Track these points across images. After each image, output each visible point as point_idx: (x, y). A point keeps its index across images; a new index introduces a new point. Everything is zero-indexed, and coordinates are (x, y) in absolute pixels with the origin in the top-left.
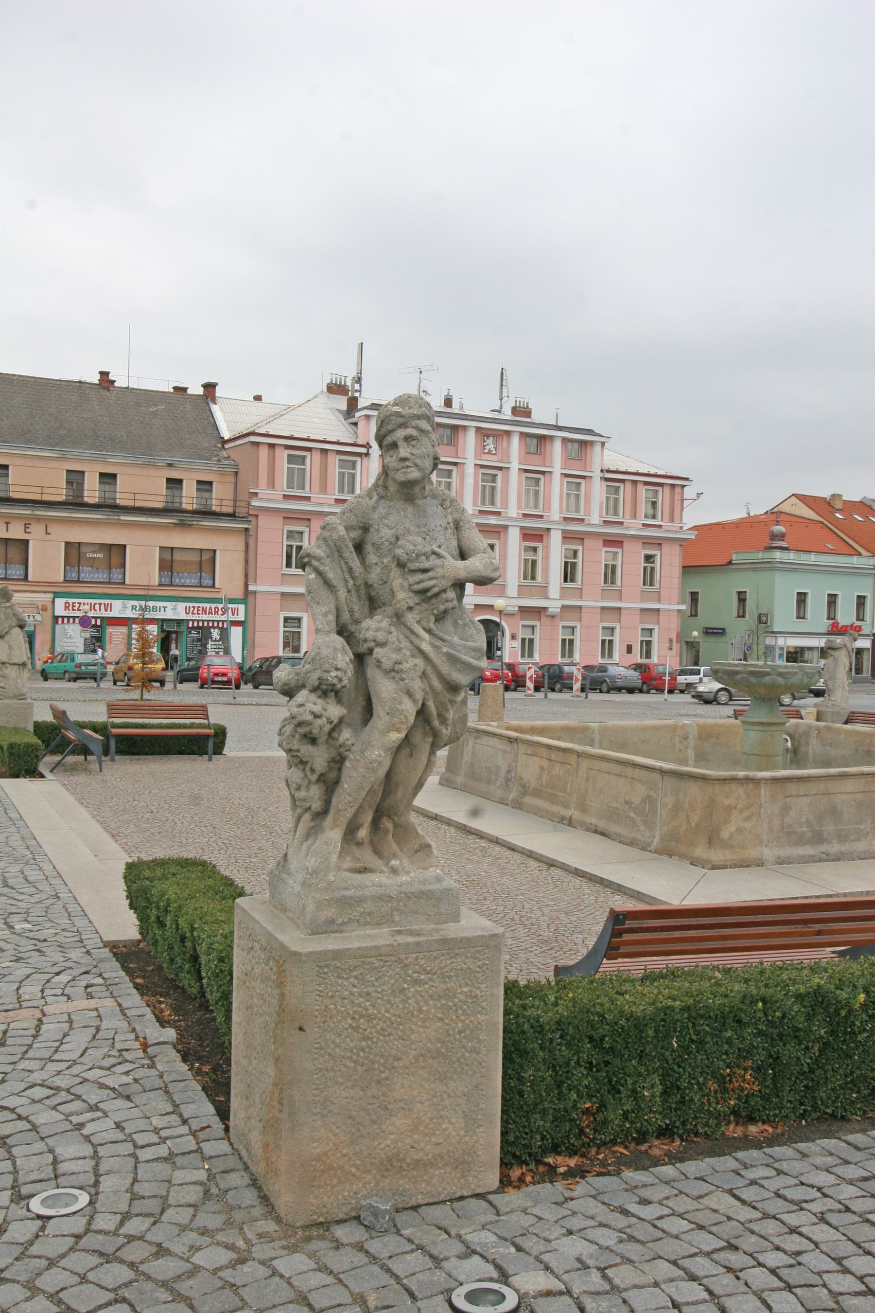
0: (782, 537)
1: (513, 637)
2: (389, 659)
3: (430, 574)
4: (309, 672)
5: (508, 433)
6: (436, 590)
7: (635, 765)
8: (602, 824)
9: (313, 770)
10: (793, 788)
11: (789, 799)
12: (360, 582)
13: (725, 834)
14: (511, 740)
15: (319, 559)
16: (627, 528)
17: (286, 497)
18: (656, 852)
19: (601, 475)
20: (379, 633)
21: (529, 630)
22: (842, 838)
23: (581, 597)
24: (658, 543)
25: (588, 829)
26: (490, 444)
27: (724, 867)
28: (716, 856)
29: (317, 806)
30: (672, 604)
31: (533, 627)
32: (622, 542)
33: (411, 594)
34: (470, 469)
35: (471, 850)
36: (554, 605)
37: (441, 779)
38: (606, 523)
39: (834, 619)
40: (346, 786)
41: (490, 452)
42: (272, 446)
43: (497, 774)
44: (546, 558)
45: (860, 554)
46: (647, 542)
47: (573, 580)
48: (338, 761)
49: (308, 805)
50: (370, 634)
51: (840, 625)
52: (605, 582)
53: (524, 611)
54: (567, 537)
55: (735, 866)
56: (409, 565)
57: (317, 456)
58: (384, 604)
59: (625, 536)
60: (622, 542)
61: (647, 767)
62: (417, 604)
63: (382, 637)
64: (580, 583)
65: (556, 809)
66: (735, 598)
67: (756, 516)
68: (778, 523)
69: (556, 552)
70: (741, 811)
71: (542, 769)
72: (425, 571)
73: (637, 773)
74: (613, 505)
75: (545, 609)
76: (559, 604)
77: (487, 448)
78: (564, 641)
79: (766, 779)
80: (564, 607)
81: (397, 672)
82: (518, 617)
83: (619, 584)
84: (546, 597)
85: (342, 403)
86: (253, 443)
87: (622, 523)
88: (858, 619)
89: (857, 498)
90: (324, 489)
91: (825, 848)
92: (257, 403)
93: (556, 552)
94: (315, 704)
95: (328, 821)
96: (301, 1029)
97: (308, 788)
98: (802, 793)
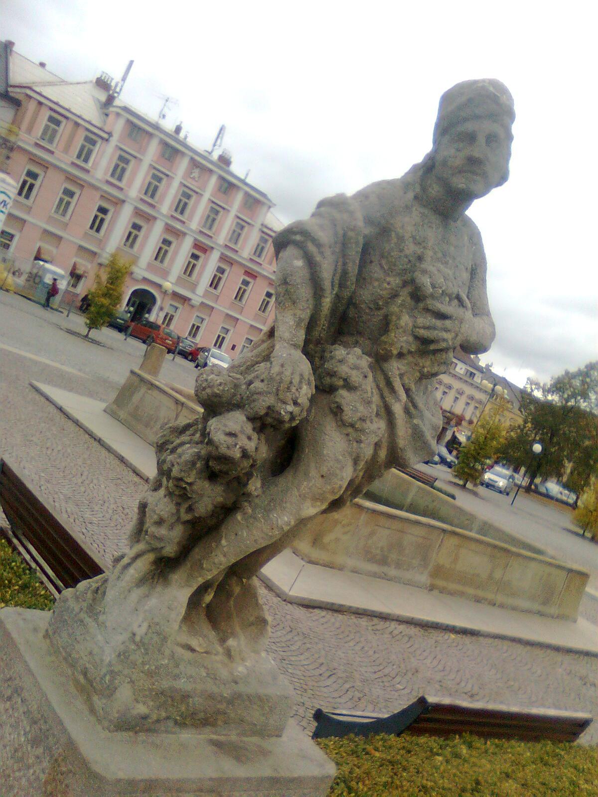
1: (161, 309)
2: (356, 410)
3: (448, 323)
4: (259, 393)
5: (211, 171)
6: (444, 345)
9: (190, 509)
10: (382, 521)
11: (377, 527)
12: (346, 294)
13: (327, 539)
14: (177, 402)
15: (319, 245)
16: (264, 269)
17: (37, 145)
19: (260, 227)
21: (174, 309)
22: (398, 566)
23: (241, 313)
24: (45, 166)
26: (196, 173)
27: (317, 564)
28: (315, 554)
29: (170, 550)
31: (177, 308)
32: (256, 277)
33: (411, 339)
34: (175, 184)
35: (126, 482)
36: (196, 300)
37: (107, 407)
40: (224, 542)
41: (193, 178)
42: (40, 103)
43: (155, 422)
44: (146, 237)
48: (226, 511)
49: (159, 545)
50: (344, 370)
52: (236, 298)
53: (175, 295)
54: (223, 258)
55: (325, 566)
56: (429, 302)
57: (70, 125)
58: (360, 333)
60: (256, 277)
62: (410, 352)
63: (357, 379)
64: (219, 292)
69: (210, 265)
70: (343, 526)
72: (442, 316)
75: (190, 300)
76: (201, 300)
77: (193, 175)
78: (194, 325)
79: (368, 509)
80: (202, 303)
81: (356, 430)
82: (170, 297)
83: (244, 303)
84: (193, 291)
85: (103, 98)
86: (27, 95)
87: (261, 264)
90: (66, 150)
91: (385, 569)
92: (41, 69)
93: (210, 265)
94: (249, 438)
95: (177, 577)
97: (172, 527)
98: (386, 526)
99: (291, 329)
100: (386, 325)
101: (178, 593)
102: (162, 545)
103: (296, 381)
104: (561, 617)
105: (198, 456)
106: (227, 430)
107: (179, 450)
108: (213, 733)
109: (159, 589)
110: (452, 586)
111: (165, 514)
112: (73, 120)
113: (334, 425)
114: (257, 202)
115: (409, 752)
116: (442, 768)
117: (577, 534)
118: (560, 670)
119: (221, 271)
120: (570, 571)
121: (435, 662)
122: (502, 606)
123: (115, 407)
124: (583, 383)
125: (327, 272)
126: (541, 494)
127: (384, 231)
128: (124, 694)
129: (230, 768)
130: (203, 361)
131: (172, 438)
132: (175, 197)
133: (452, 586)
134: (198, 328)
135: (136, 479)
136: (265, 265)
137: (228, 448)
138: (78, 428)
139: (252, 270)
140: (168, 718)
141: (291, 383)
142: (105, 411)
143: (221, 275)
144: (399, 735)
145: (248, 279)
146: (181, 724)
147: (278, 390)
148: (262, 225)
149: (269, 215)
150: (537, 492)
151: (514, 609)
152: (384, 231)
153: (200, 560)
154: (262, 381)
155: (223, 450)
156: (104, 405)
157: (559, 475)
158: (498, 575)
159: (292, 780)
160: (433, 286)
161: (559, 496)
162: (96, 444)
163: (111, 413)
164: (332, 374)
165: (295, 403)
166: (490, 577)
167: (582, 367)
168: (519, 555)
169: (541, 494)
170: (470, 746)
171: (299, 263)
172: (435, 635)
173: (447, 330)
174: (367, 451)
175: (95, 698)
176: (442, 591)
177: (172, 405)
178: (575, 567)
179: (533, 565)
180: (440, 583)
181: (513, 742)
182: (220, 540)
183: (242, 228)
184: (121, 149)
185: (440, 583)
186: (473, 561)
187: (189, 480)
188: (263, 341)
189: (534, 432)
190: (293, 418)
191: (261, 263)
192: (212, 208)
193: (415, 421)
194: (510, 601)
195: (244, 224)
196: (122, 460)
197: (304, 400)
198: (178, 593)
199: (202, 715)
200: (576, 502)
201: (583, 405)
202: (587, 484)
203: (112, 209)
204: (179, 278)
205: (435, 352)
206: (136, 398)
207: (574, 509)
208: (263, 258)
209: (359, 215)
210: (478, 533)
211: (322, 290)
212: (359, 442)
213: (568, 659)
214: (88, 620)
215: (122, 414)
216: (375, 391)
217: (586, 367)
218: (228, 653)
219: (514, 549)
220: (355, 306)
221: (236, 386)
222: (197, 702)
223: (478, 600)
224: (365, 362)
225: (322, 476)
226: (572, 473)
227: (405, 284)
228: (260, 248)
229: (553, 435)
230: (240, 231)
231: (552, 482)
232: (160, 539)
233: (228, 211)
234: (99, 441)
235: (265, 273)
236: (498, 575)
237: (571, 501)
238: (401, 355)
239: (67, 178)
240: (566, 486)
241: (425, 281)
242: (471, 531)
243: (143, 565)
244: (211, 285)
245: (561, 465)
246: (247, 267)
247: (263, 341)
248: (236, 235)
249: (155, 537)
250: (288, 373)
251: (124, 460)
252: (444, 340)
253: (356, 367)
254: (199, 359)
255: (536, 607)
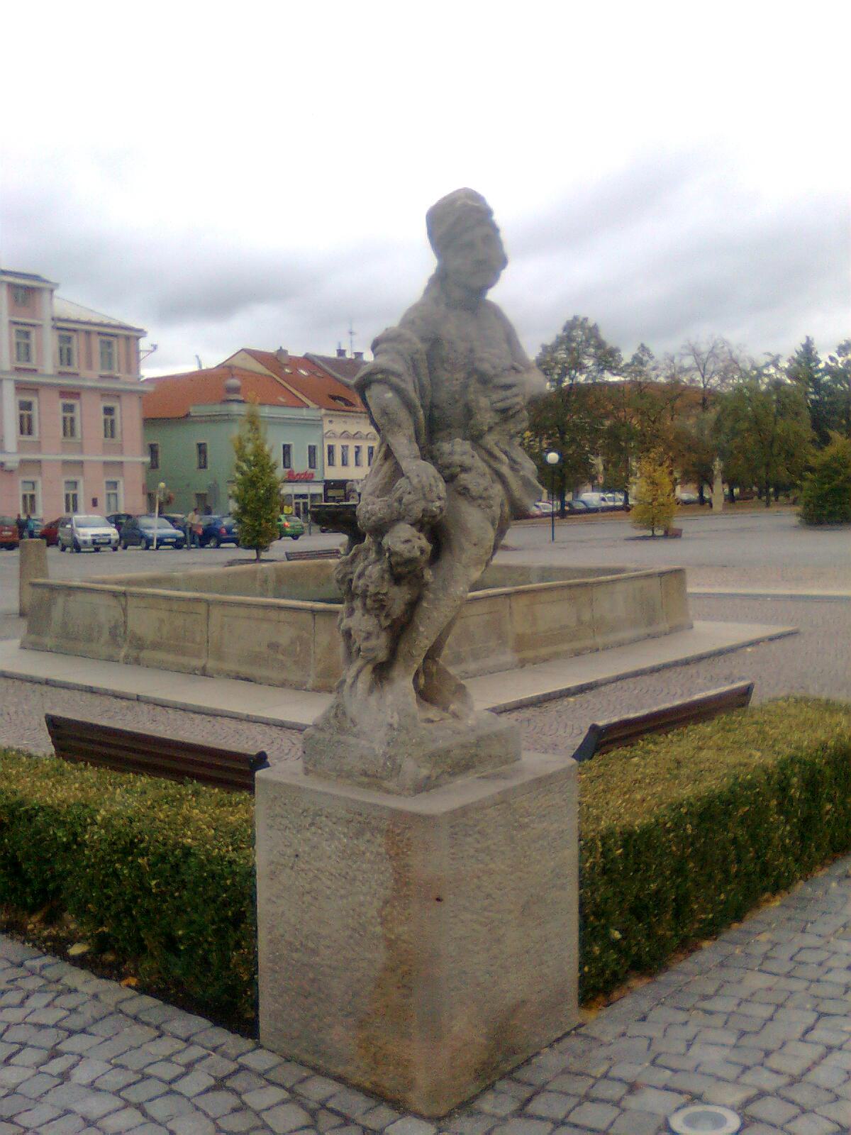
0: (236, 390)
2: (478, 485)
3: (515, 390)
6: (518, 407)
7: (280, 608)
8: (245, 670)
12: (428, 401)
14: (115, 594)
15: (399, 376)
16: (84, 379)
18: (313, 690)
19: (52, 323)
20: (464, 457)
22: (475, 656)
23: (82, 452)
24: (117, 395)
25: (228, 676)
29: (382, 655)
30: (136, 457)
33: (492, 414)
38: (61, 374)
39: (289, 467)
40: (421, 629)
45: (308, 407)
46: (106, 394)
47: (30, 433)
48: (413, 605)
50: (457, 459)
51: (295, 474)
52: (65, 434)
54: (21, 388)
58: (449, 426)
59: (81, 387)
61: (286, 608)
62: (496, 424)
65: (184, 660)
66: (195, 451)
67: (209, 370)
68: (233, 376)
71: (162, 621)
72: (508, 387)
73: (283, 615)
74: (65, 356)
76: (17, 458)
78: (25, 497)
80: (23, 462)
88: (310, 467)
89: (300, 354)
94: (419, 539)
95: (396, 672)
96: (438, 900)
99: (405, 446)
100: (469, 413)
101: (403, 685)
102: (374, 655)
103: (433, 481)
104: (674, 630)
105: (383, 571)
106: (403, 540)
107: (367, 573)
108: (476, 773)
109: (387, 688)
110: (544, 651)
111: (370, 628)
112: (83, 330)
113: (466, 502)
114: (30, 290)
115: (607, 765)
116: (642, 763)
117: (645, 538)
118: (700, 681)
119: (26, 406)
120: (661, 574)
121: (569, 730)
122: (606, 648)
123: (33, 637)
124: (570, 351)
125: (410, 387)
126: (580, 512)
127: (435, 342)
128: (409, 765)
129: (503, 785)
130: (69, 538)
131: (349, 569)
132: (10, 342)
133: (544, 651)
134: (32, 497)
135: (124, 703)
136: (84, 372)
137: (409, 552)
138: (10, 681)
139: (68, 386)
140: (443, 772)
141: (430, 485)
142: (23, 647)
143: (29, 412)
144: (591, 758)
145: (69, 401)
146: (453, 774)
147: (424, 495)
148: (53, 319)
149: (56, 301)
150: (574, 512)
151: (620, 644)
152: (435, 342)
153: (409, 651)
154: (410, 493)
155: (407, 555)
156: (17, 642)
157: (593, 479)
158: (586, 616)
159: (550, 776)
160: (494, 368)
161: (603, 504)
162: (45, 688)
163: (32, 646)
164: (449, 466)
165: (440, 499)
166: (580, 622)
167: (560, 332)
168: (600, 583)
169: (580, 512)
170: (655, 743)
171: (390, 395)
172: (554, 707)
173: (516, 395)
174: (497, 511)
175: (386, 784)
176: (535, 661)
177: (112, 602)
178: (664, 568)
179: (619, 587)
180: (529, 654)
181: (690, 727)
182: (418, 628)
183: (27, 335)
184: (16, 323)
185: (529, 654)
186: (554, 613)
187: (384, 591)
188: (382, 465)
189: (537, 439)
190: (441, 510)
191: (34, 367)
192: (18, 331)
193: (521, 473)
194: (612, 638)
195: (25, 328)
196: (91, 690)
197: (443, 494)
198: (403, 685)
199: (463, 762)
200: (626, 500)
201: (581, 378)
202: (630, 473)
203: (34, 399)
204: (19, 443)
205: (513, 416)
206: (57, 613)
207: (628, 510)
208: (76, 365)
209: (415, 339)
210: (540, 581)
211: (415, 407)
212: (491, 507)
213: (702, 666)
214: (342, 738)
215: (49, 641)
216: (484, 465)
217: (565, 329)
218: (455, 715)
219: (591, 580)
220: (437, 407)
221: (389, 506)
222: (456, 752)
223: (578, 653)
224: (467, 446)
225: (475, 545)
226: (605, 469)
227: (469, 375)
228: (65, 351)
229: (563, 433)
230: (26, 341)
231: (587, 492)
232: (372, 650)
233: (40, 326)
234: (47, 682)
235: (89, 384)
236: (586, 616)
237: (620, 504)
238: (490, 429)
239: (103, 395)
240: (607, 488)
241: (486, 367)
242: (531, 583)
243: (366, 677)
244: (22, 432)
245: (587, 466)
246: (59, 385)
247: (382, 465)
248: (22, 349)
249: (368, 650)
250: (424, 479)
251: (94, 690)
252: (518, 403)
253: (465, 453)
254: (62, 537)
255: (643, 631)
